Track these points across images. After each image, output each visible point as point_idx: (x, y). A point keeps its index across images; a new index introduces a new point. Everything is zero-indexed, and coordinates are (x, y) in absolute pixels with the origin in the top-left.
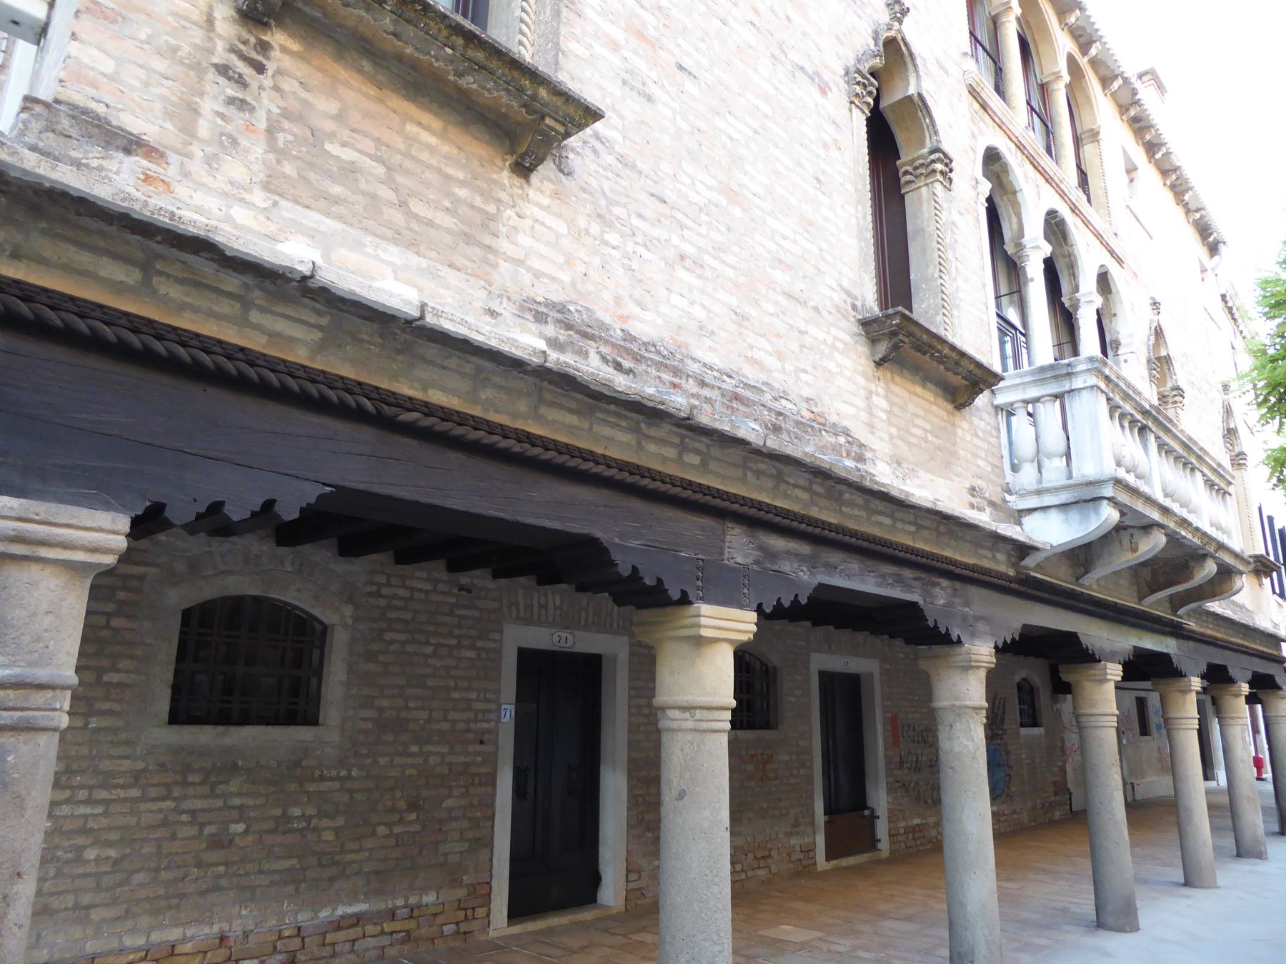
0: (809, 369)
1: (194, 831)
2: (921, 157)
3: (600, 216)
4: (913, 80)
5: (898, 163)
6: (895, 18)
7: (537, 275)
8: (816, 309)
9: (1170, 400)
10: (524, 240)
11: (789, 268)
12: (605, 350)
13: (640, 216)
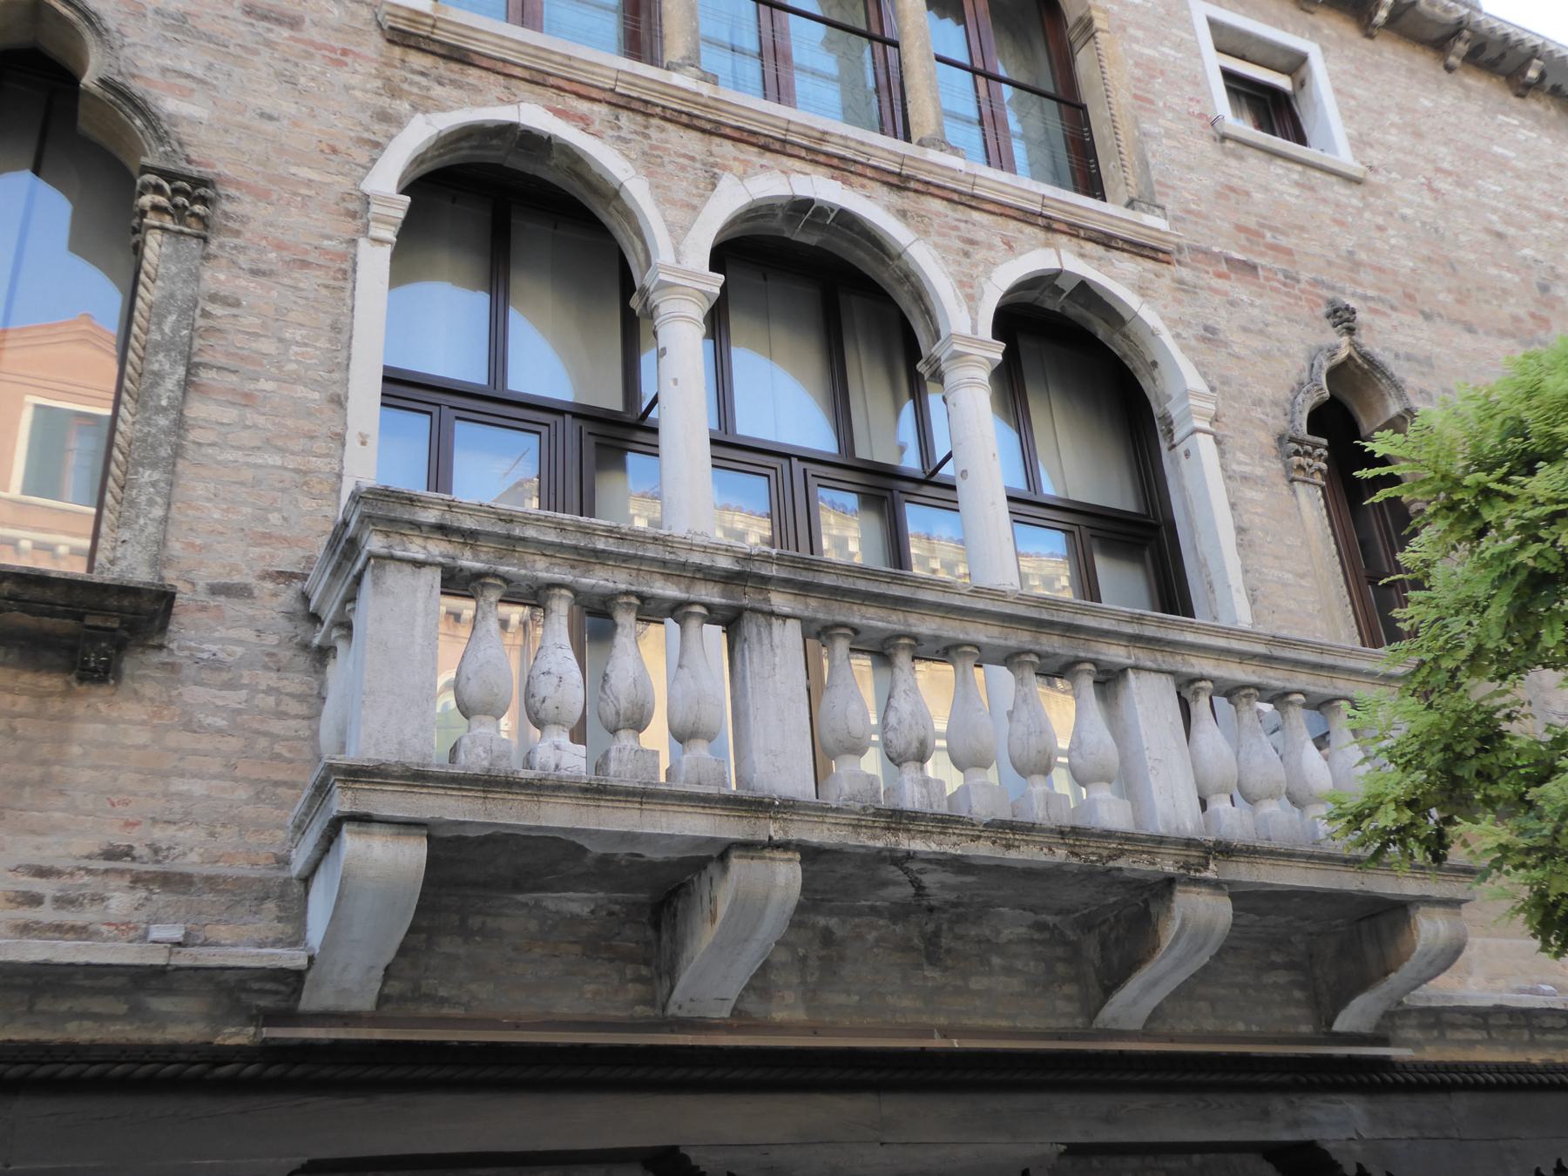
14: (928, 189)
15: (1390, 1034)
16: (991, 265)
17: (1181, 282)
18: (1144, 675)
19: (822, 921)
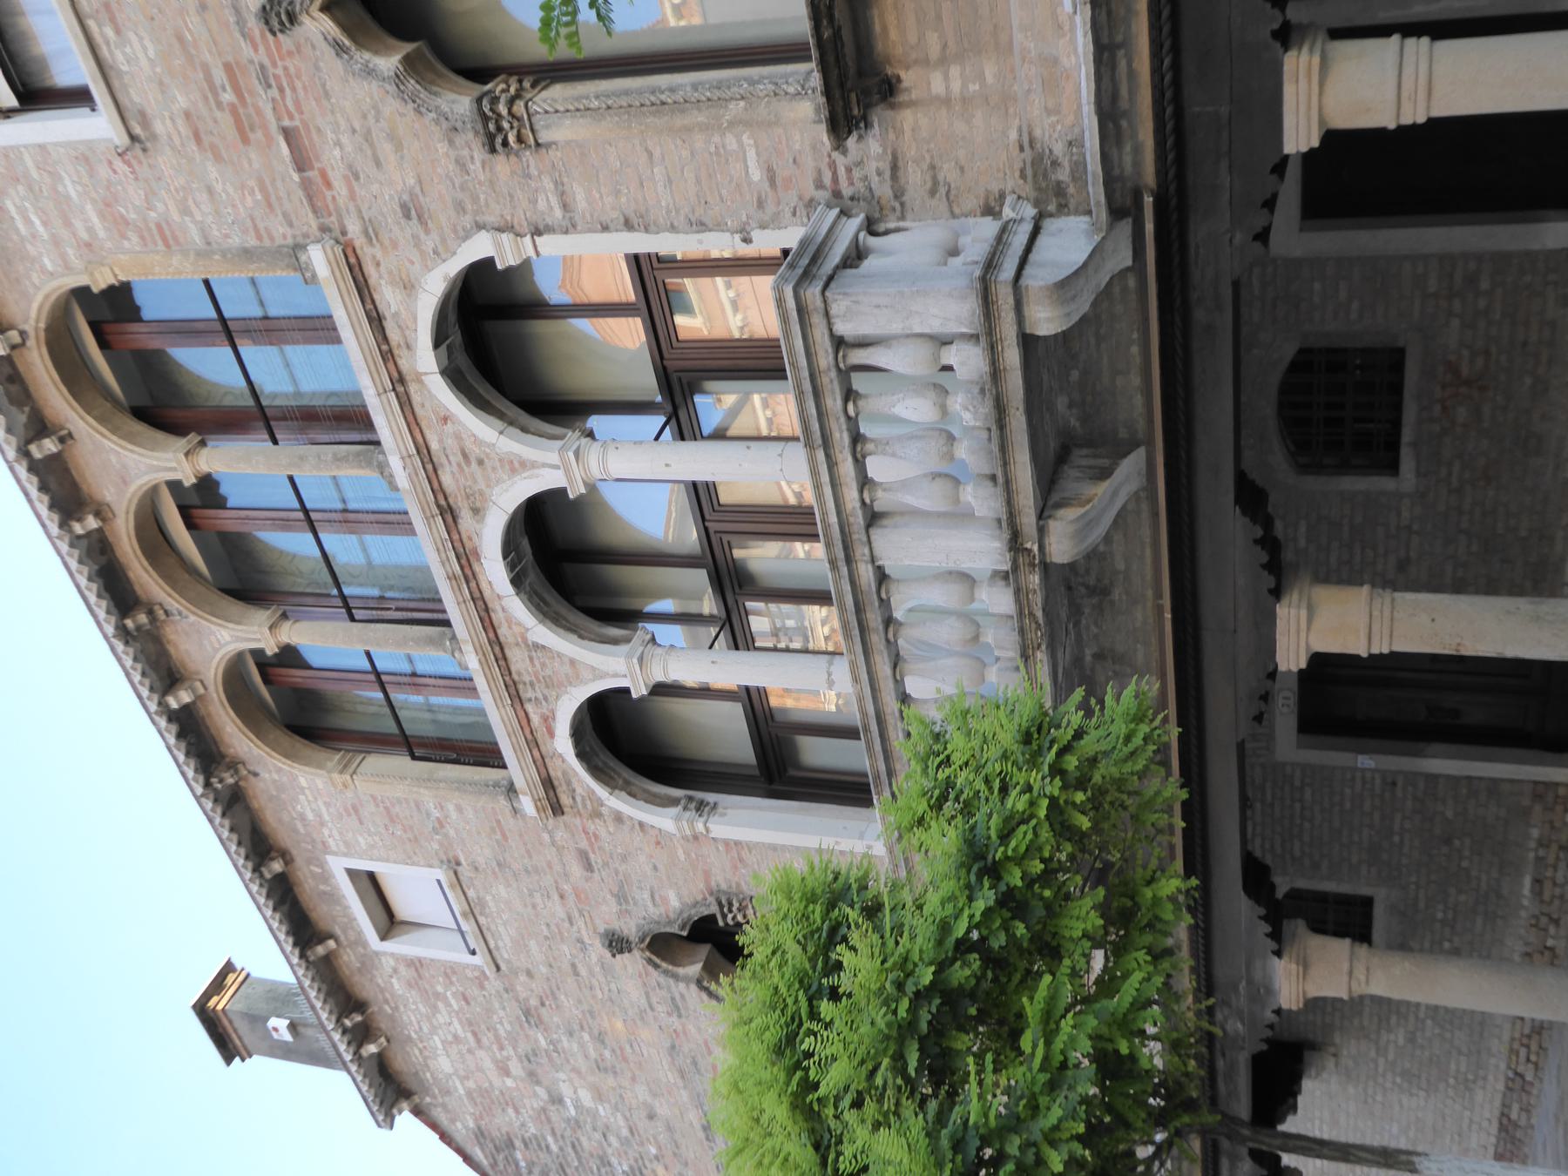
14: (438, 490)
15: (1129, 184)
18: (877, 552)
19: (1088, 658)
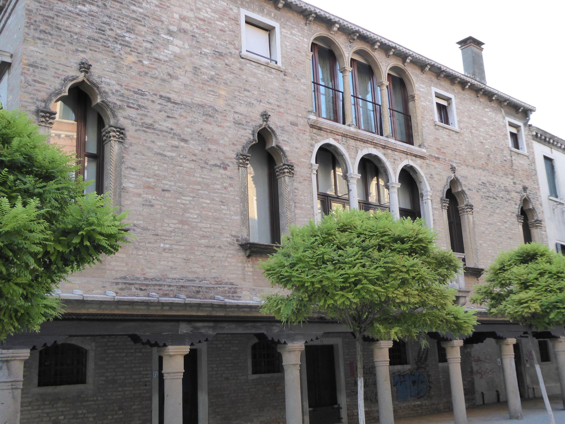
0: (215, 268)
1: (48, 419)
2: (281, 166)
3: (136, 248)
4: (274, 140)
5: (275, 167)
6: (264, 121)
7: (117, 271)
8: (220, 247)
9: (465, 211)
10: (113, 263)
11: (208, 237)
12: (136, 286)
13: (149, 243)
14: (389, 148)
16: (398, 165)
17: (427, 164)
